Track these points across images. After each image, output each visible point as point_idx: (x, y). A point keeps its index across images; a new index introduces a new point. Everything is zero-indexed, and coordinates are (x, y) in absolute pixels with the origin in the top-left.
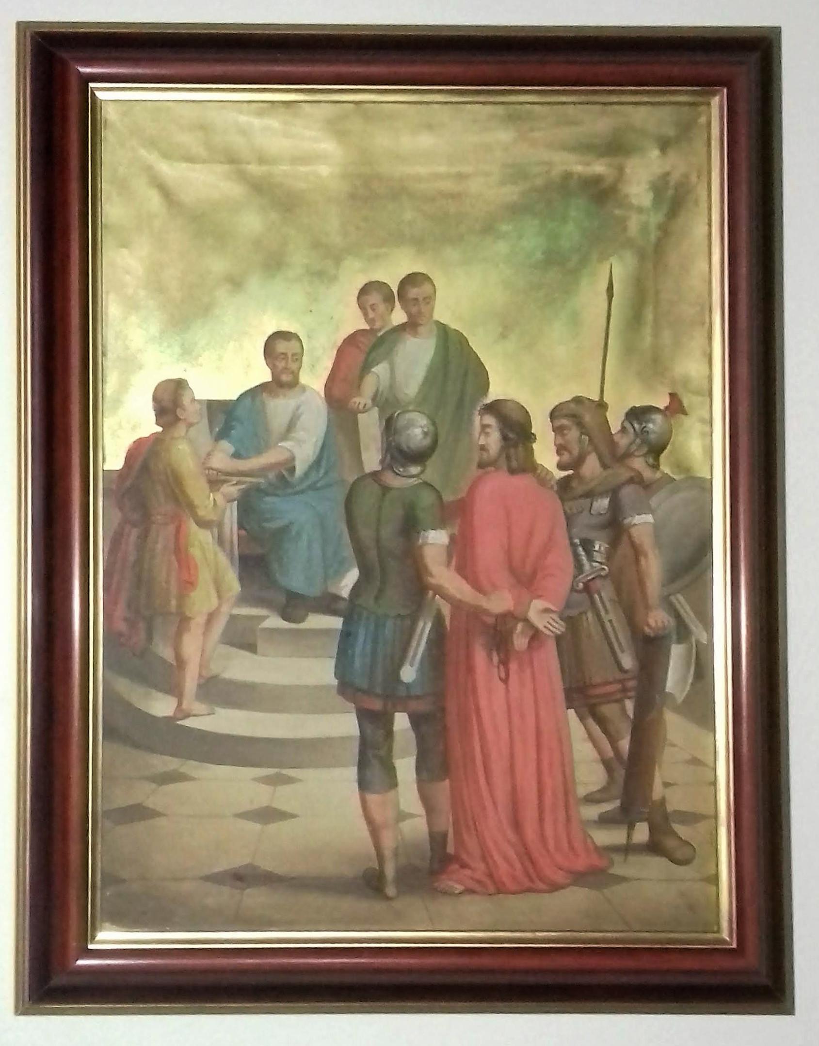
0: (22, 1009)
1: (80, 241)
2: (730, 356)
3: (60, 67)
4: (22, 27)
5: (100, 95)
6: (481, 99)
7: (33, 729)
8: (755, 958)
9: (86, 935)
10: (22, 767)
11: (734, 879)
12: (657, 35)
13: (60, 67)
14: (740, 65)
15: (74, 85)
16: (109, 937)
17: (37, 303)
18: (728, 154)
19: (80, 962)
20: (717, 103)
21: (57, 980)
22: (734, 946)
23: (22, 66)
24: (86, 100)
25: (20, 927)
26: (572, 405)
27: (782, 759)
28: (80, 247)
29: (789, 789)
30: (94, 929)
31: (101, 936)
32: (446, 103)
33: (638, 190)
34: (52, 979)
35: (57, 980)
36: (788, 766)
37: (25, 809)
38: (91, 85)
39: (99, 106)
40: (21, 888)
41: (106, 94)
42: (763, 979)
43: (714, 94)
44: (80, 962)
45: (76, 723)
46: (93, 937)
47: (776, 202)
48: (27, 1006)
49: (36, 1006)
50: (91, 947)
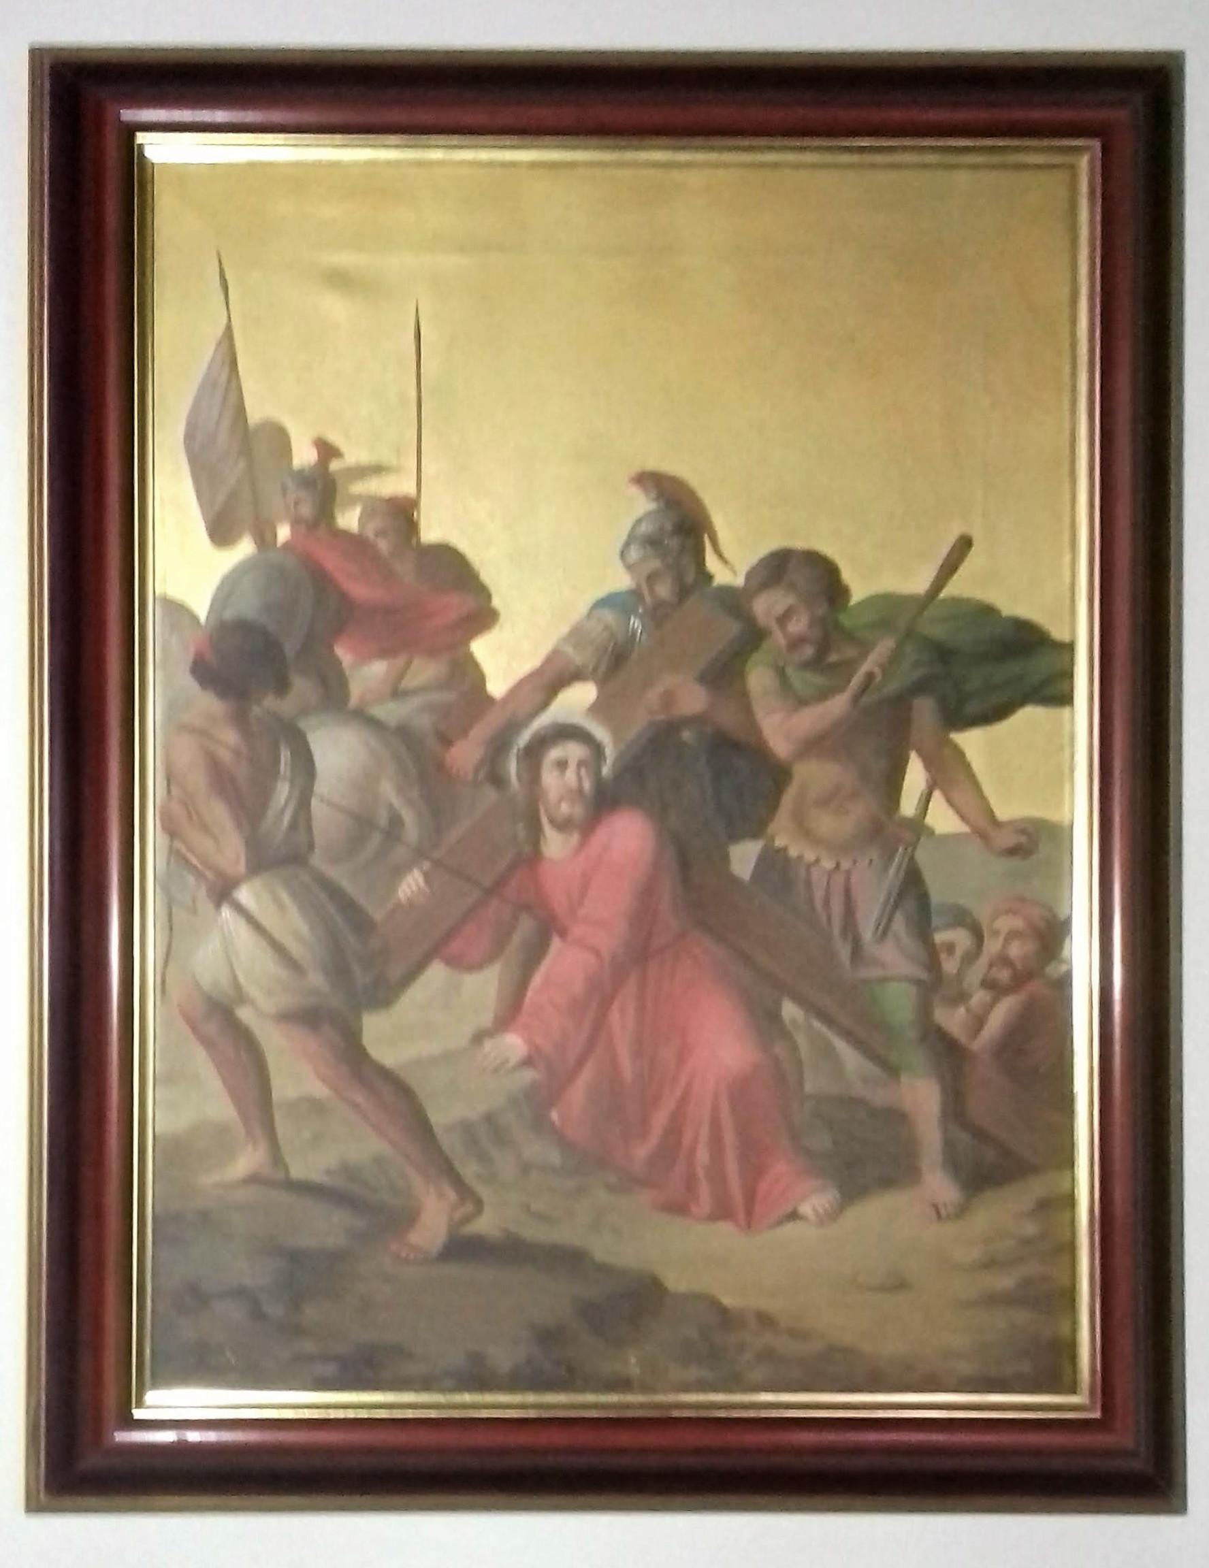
0: (34, 1506)
2: (1102, 1320)
3: (89, 110)
4: (37, 55)
7: (49, 1239)
8: (1127, 1436)
11: (1097, 1262)
13: (89, 110)
17: (57, 868)
18: (1102, 358)
21: (90, 1461)
27: (1173, 352)
29: (1182, 232)
31: (151, 1397)
34: (82, 1460)
35: (90, 1461)
39: (150, 171)
45: (113, 1115)
46: (140, 1404)
47: (1174, 1239)
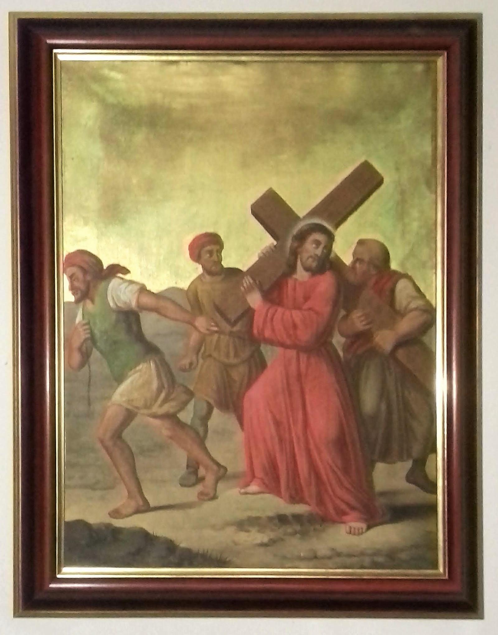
1: (100, 44)
3: (34, 37)
5: (61, 58)
10: (16, 472)
13: (34, 37)
14: (459, 37)
19: (52, 586)
20: (441, 62)
21: (39, 596)
22: (447, 577)
23: (12, 38)
32: (204, 61)
35: (39, 596)
38: (55, 51)
40: (16, 546)
41: (63, 56)
42: (464, 598)
43: (440, 55)
44: (52, 586)
48: (20, 611)
49: (27, 612)
50: (59, 576)
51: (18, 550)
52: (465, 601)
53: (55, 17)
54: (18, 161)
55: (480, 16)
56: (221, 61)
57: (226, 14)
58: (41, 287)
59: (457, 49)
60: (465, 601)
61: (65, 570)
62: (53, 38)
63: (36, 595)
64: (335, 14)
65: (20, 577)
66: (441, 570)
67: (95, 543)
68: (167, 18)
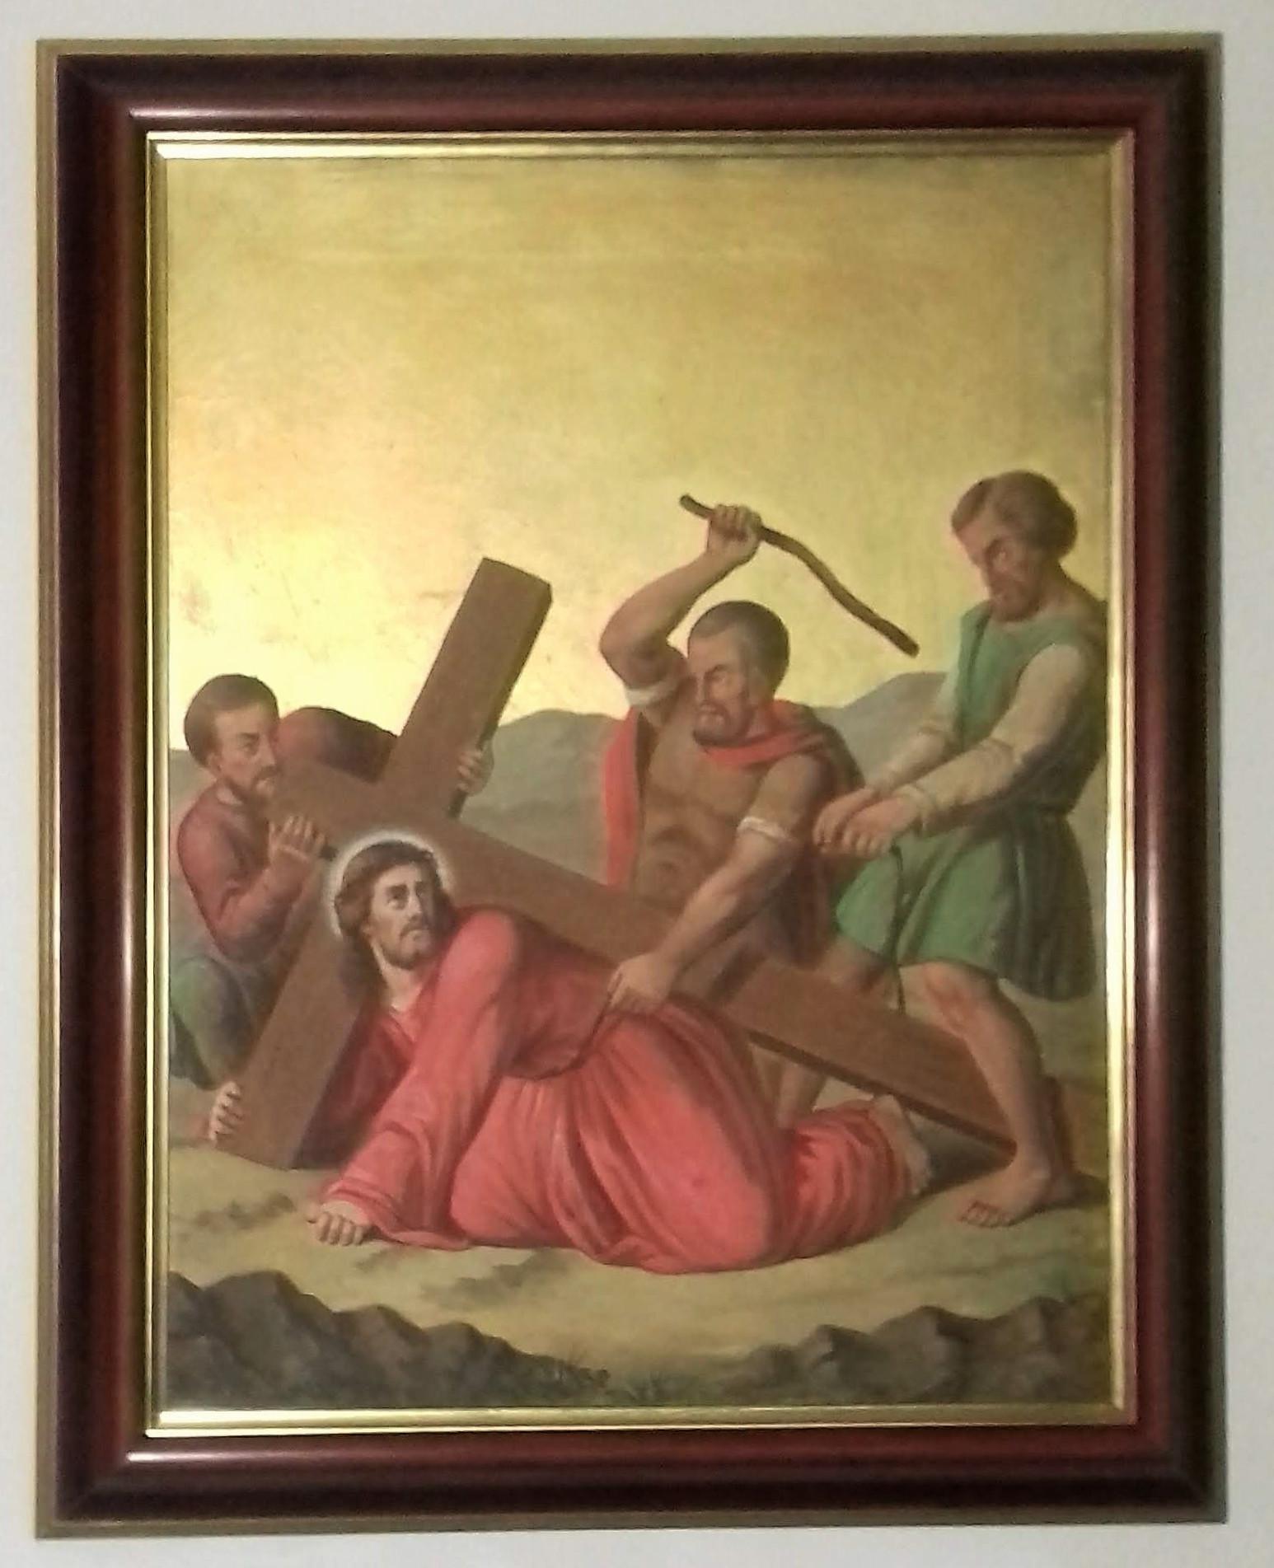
5: (164, 151)
6: (835, 149)
9: (142, 1418)
12: (1168, 47)
13: (98, 110)
14: (1156, 98)
15: (124, 134)
16: (178, 1421)
19: (135, 1457)
21: (103, 1484)
24: (141, 153)
25: (44, 200)
26: (1001, 564)
28: (93, 1518)
30: (157, 1409)
33: (630, 1242)
36: (1221, 1235)
37: (52, 622)
38: (151, 136)
41: (171, 149)
44: (135, 1457)
46: (155, 1420)
50: (151, 1433)
51: (51, 603)
52: (1175, 1474)
53: (1070, 48)
54: (56, 345)
55: (1215, 40)
56: (576, 157)
57: (735, 41)
58: (113, 735)
59: (1157, 122)
60: (1175, 1474)
61: (166, 1417)
62: (142, 106)
63: (89, 1475)
64: (1059, 38)
65: (56, 1246)
66: (1119, 1402)
67: (246, 1337)
68: (1106, 47)
